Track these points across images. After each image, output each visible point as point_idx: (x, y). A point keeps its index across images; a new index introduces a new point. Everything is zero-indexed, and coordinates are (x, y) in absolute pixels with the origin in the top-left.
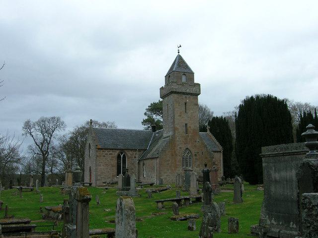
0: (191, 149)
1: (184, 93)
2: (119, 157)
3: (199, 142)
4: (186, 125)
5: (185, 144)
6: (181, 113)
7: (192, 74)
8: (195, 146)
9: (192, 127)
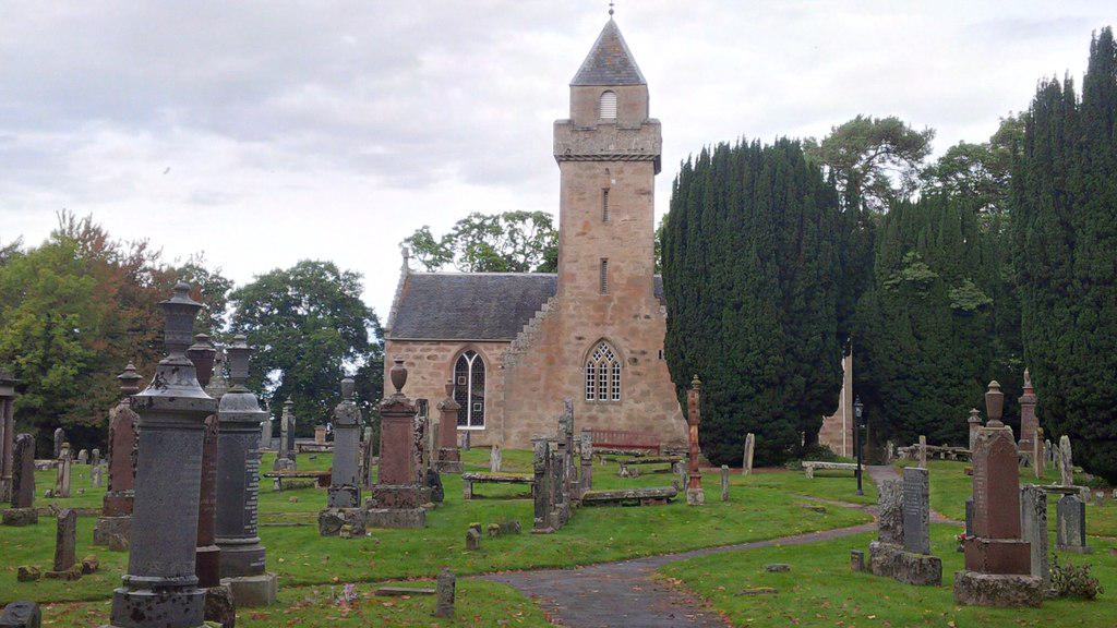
0: (619, 340)
1: (600, 159)
2: (461, 365)
3: (647, 317)
4: (604, 262)
5: (597, 325)
6: (586, 225)
7: (264, 279)
8: (634, 332)
9: (628, 270)
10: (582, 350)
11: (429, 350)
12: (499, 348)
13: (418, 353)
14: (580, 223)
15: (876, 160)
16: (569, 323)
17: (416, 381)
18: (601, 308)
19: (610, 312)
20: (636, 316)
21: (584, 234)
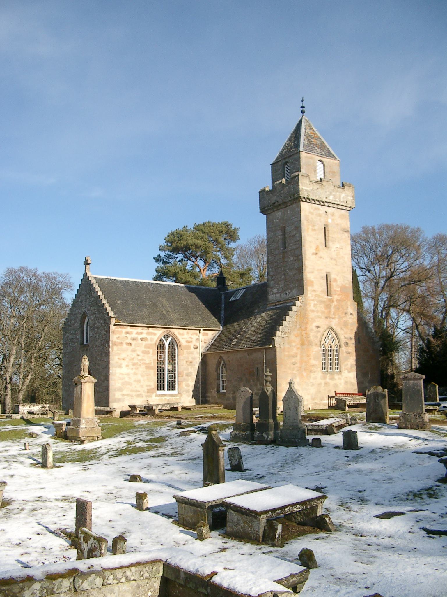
2: (161, 346)
3: (352, 314)
5: (326, 318)
6: (317, 248)
10: (319, 335)
11: (141, 333)
12: (188, 333)
13: (134, 335)
14: (314, 247)
15: (248, 259)
16: (312, 315)
17: (132, 357)
18: (328, 307)
19: (333, 310)
20: (346, 314)
21: (316, 254)
